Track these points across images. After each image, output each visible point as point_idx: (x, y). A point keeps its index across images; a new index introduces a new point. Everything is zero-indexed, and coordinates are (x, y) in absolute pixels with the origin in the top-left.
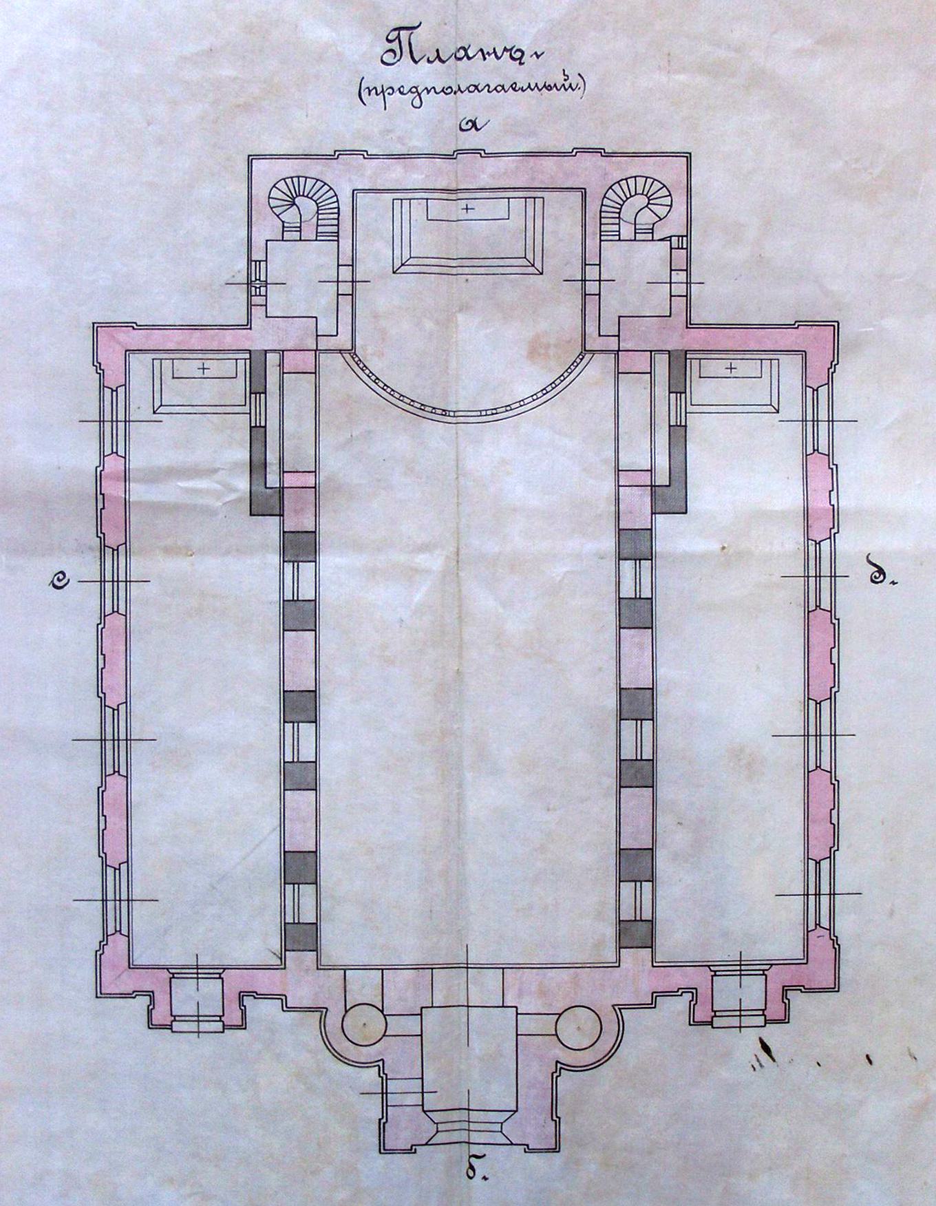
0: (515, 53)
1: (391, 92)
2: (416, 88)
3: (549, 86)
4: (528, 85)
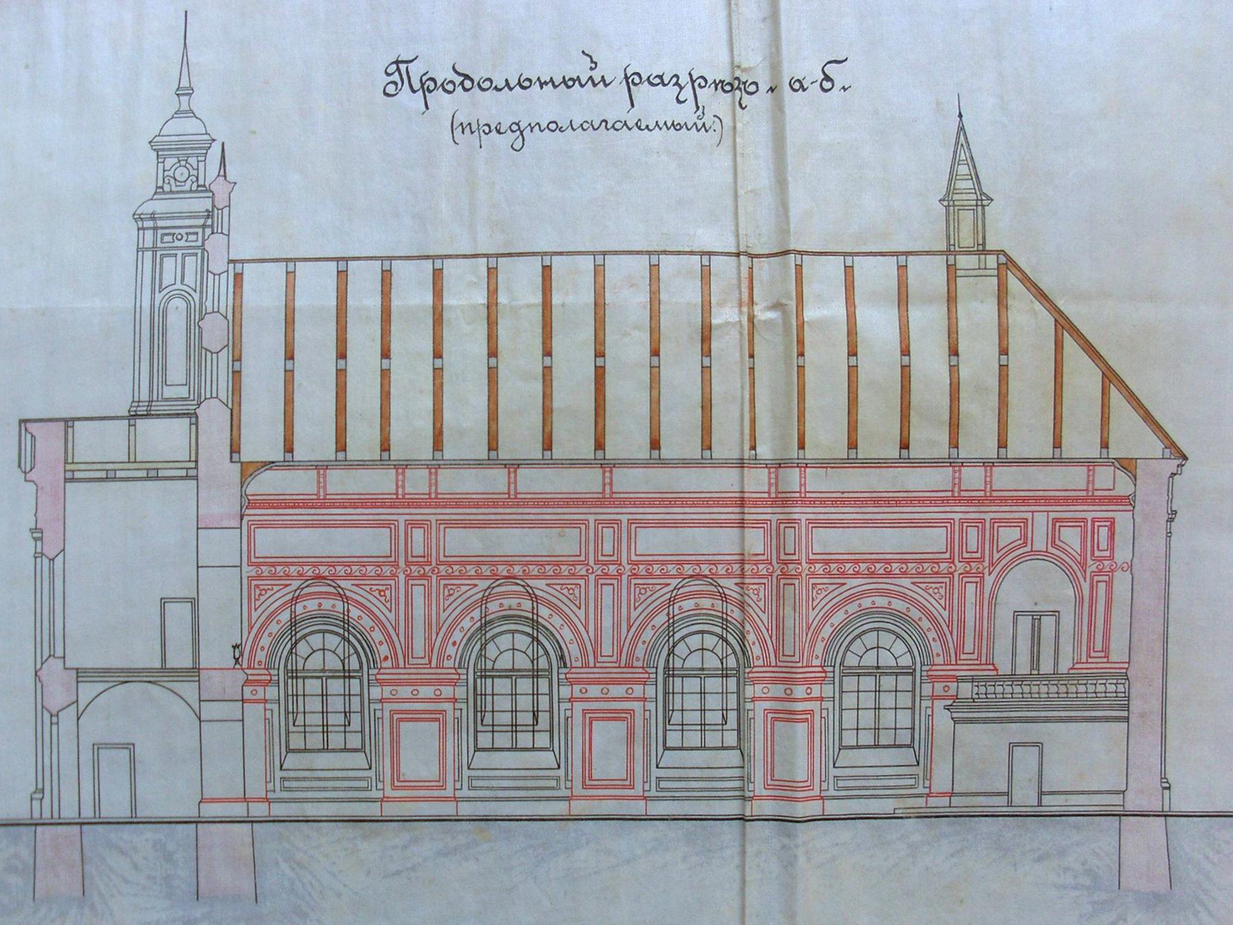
0: (483, 82)
1: (487, 130)
2: (517, 124)
3: (679, 124)
4: (534, 130)
